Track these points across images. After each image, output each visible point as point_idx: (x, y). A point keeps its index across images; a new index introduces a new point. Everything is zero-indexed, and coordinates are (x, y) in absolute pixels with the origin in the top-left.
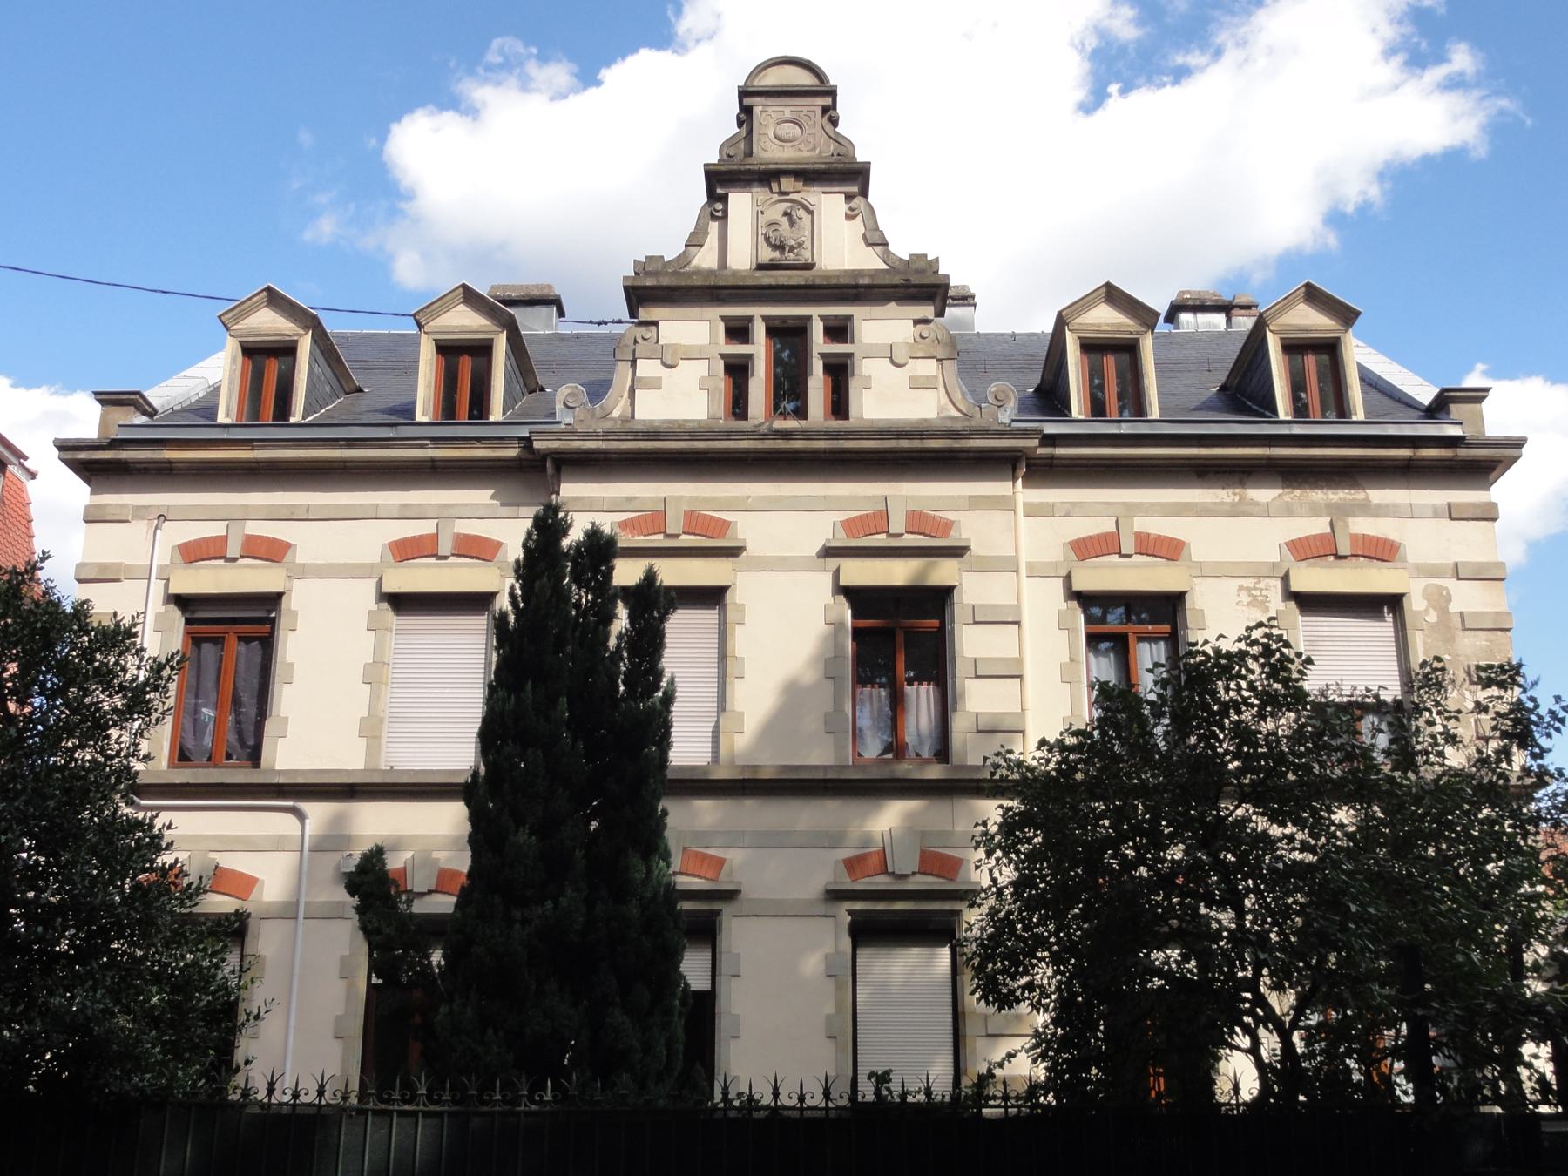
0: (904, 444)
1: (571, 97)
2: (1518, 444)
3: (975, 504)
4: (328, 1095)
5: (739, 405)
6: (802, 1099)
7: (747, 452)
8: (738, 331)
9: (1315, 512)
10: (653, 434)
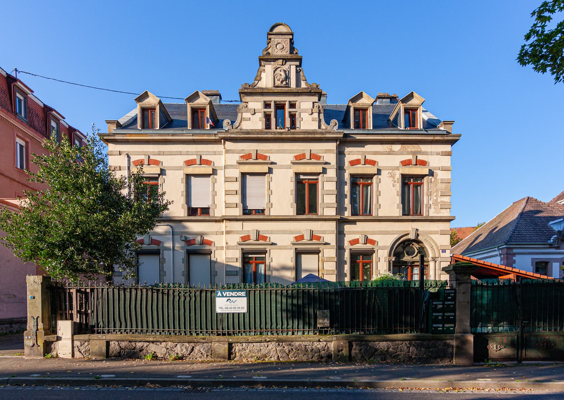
0: (310, 136)
1: (528, 32)
2: (460, 136)
3: (278, 152)
4: (363, 286)
5: (268, 126)
6: (388, 286)
7: (271, 138)
8: (267, 105)
9: (408, 153)
10: (248, 133)
